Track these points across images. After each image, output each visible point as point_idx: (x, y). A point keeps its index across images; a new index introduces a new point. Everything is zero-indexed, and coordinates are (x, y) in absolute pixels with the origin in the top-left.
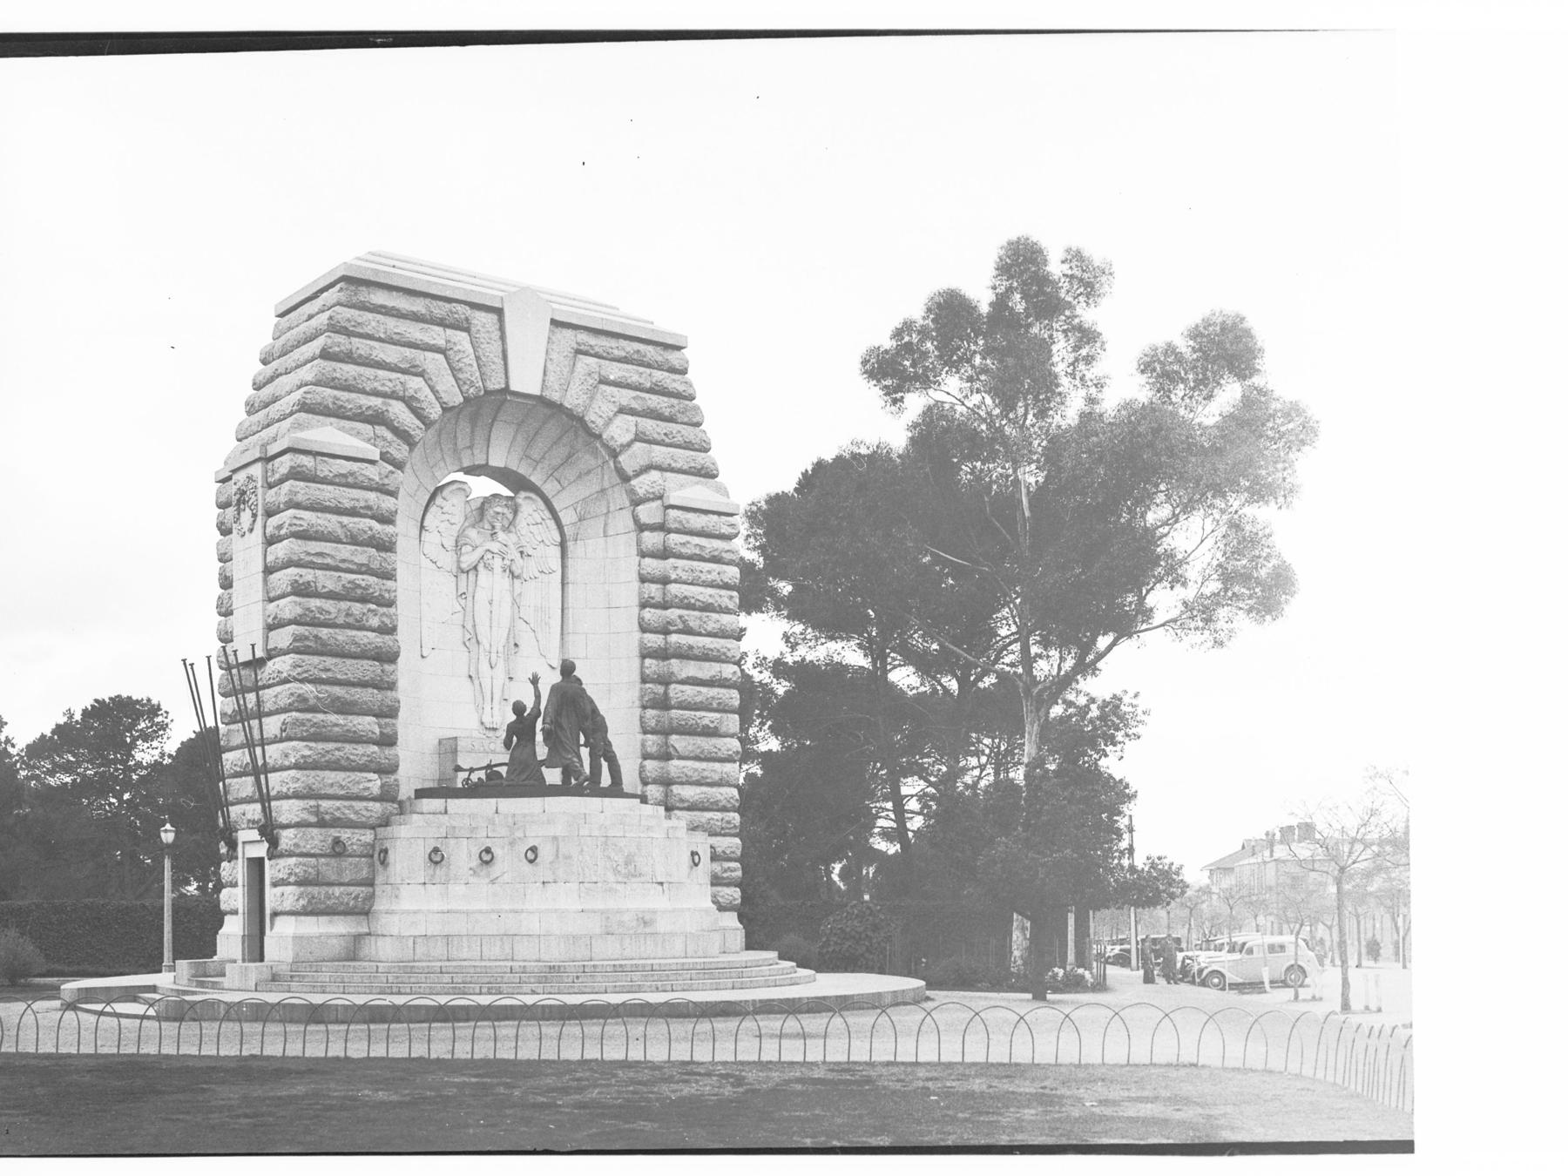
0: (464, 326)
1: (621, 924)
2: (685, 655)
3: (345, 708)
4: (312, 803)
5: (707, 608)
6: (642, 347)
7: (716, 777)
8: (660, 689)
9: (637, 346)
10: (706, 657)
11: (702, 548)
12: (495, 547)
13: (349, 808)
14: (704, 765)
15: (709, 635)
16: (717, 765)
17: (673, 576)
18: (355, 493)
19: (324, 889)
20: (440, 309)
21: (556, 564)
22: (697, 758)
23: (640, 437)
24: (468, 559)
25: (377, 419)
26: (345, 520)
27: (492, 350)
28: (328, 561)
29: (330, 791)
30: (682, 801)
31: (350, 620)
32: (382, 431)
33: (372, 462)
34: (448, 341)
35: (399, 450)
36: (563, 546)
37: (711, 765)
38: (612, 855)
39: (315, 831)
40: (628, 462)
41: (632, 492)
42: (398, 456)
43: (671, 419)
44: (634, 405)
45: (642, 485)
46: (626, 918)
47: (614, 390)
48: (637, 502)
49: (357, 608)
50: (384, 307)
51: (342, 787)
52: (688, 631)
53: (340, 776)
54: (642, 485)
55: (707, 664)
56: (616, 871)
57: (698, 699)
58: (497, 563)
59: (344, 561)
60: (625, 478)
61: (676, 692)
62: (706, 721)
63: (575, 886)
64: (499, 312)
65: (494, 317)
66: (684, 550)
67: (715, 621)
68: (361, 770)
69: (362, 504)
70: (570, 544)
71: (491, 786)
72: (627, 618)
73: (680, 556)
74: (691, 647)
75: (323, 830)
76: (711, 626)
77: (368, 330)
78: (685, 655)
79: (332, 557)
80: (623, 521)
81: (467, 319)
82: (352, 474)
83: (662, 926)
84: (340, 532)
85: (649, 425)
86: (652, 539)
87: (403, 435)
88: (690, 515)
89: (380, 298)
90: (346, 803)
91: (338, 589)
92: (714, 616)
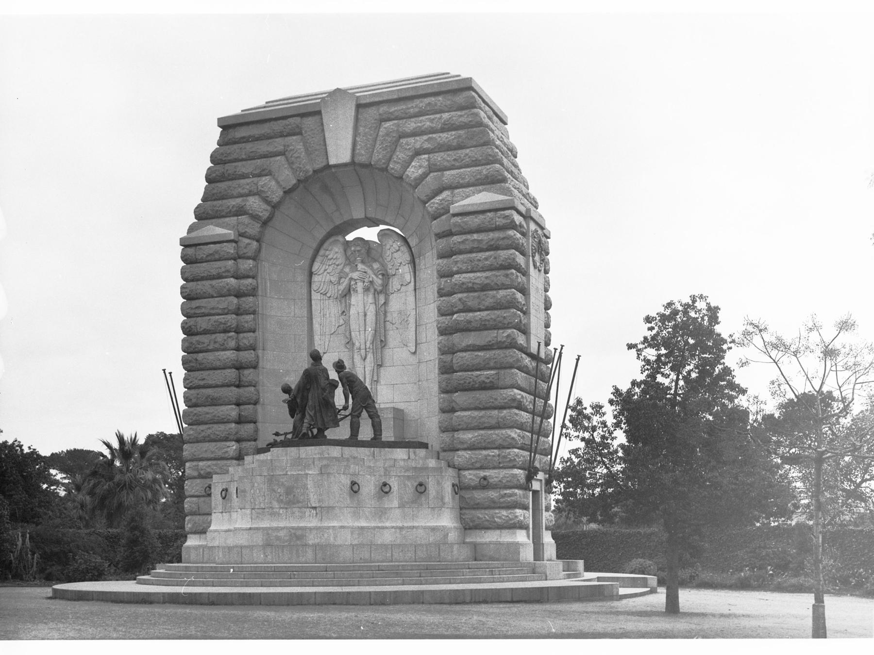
0: (297, 132)
1: (278, 538)
4: (195, 463)
5: (485, 288)
7: (493, 422)
10: (484, 327)
11: (479, 241)
12: (355, 275)
13: (216, 465)
14: (483, 413)
15: (487, 309)
16: (495, 413)
17: (455, 269)
18: (218, 264)
19: (201, 518)
20: (277, 126)
21: (408, 277)
22: (476, 409)
23: (433, 168)
26: (214, 282)
28: (203, 310)
29: (205, 455)
30: (462, 443)
31: (217, 346)
34: (284, 146)
36: (413, 262)
37: (488, 412)
38: (276, 488)
39: (198, 481)
43: (460, 147)
44: (426, 145)
46: (281, 534)
49: (220, 337)
50: (244, 138)
51: (212, 452)
53: (212, 446)
55: (486, 332)
56: (280, 501)
57: (476, 361)
59: (213, 308)
62: (482, 378)
63: (248, 511)
66: (462, 247)
67: (491, 297)
68: (222, 441)
69: (223, 270)
70: (417, 261)
71: (285, 444)
73: (461, 252)
74: (469, 322)
75: (202, 480)
76: (489, 302)
77: (235, 156)
79: (205, 307)
81: (298, 126)
82: (216, 252)
83: (312, 539)
84: (210, 291)
85: (439, 157)
88: (467, 219)
90: (214, 462)
91: (209, 327)
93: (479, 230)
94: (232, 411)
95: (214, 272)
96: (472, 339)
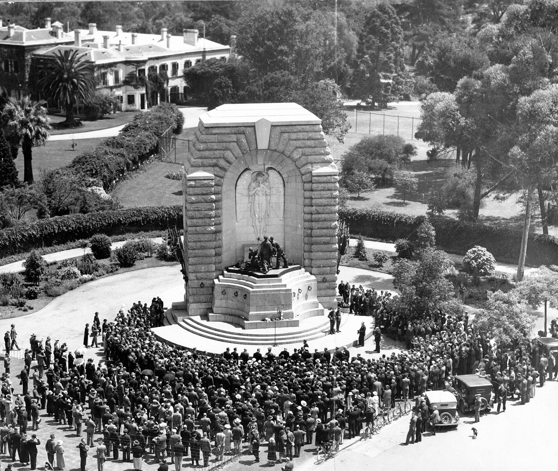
0: (227, 149)
2: (318, 221)
3: (203, 248)
6: (304, 127)
8: (310, 231)
9: (302, 127)
21: (282, 189)
23: (304, 154)
24: (252, 193)
25: (215, 165)
26: (204, 197)
27: (252, 138)
32: (217, 169)
33: (212, 180)
35: (221, 173)
40: (299, 163)
41: (300, 172)
42: (221, 175)
45: (303, 170)
47: (295, 142)
48: (302, 175)
52: (318, 213)
54: (303, 170)
58: (260, 193)
60: (299, 168)
61: (315, 232)
64: (254, 127)
65: (252, 129)
72: (300, 208)
78: (318, 221)
80: (299, 179)
86: (307, 186)
87: (221, 168)
88: (319, 178)
89: (215, 131)
92: (329, 207)
93: (324, 183)
94: (213, 252)
95: (204, 192)
96: (320, 225)
